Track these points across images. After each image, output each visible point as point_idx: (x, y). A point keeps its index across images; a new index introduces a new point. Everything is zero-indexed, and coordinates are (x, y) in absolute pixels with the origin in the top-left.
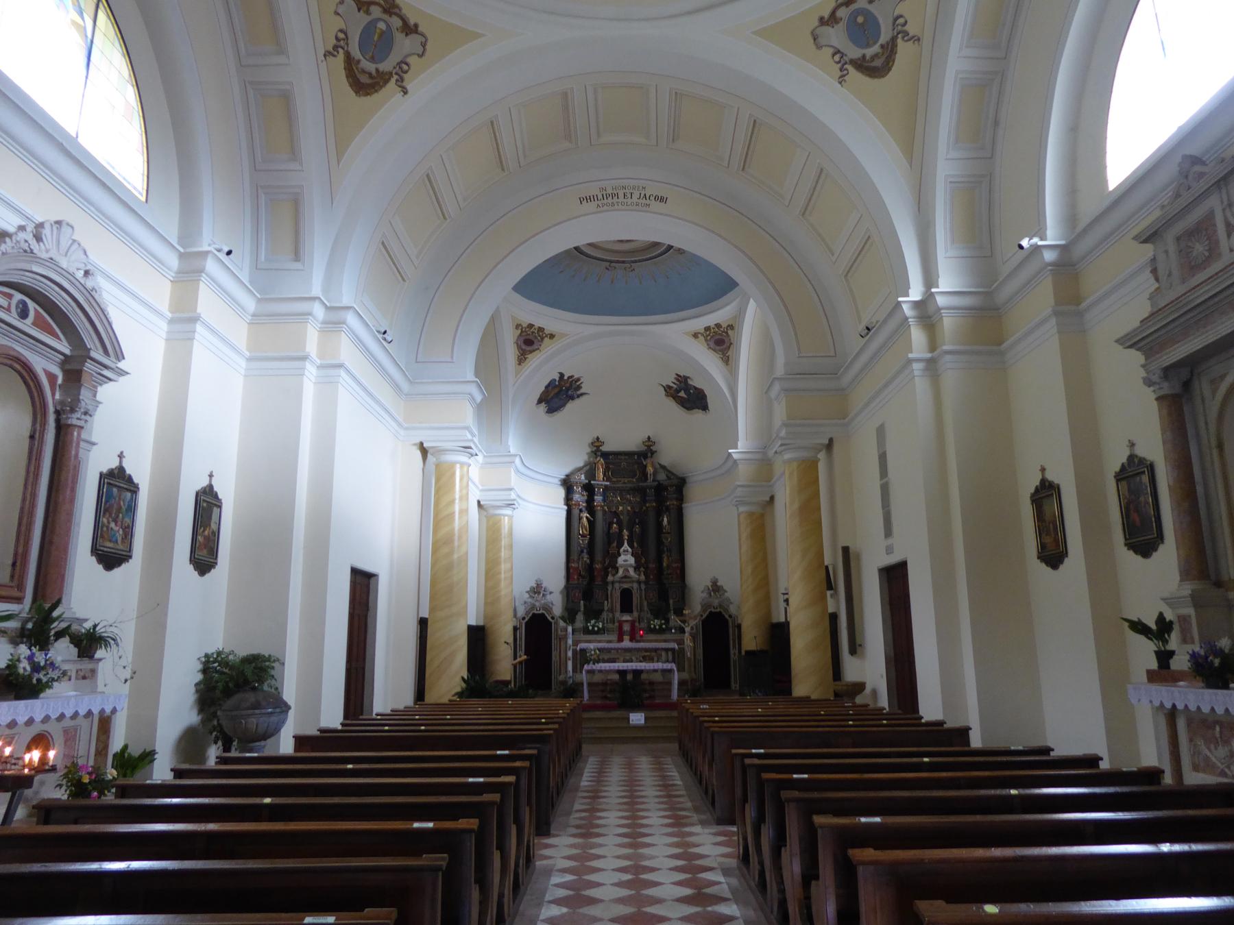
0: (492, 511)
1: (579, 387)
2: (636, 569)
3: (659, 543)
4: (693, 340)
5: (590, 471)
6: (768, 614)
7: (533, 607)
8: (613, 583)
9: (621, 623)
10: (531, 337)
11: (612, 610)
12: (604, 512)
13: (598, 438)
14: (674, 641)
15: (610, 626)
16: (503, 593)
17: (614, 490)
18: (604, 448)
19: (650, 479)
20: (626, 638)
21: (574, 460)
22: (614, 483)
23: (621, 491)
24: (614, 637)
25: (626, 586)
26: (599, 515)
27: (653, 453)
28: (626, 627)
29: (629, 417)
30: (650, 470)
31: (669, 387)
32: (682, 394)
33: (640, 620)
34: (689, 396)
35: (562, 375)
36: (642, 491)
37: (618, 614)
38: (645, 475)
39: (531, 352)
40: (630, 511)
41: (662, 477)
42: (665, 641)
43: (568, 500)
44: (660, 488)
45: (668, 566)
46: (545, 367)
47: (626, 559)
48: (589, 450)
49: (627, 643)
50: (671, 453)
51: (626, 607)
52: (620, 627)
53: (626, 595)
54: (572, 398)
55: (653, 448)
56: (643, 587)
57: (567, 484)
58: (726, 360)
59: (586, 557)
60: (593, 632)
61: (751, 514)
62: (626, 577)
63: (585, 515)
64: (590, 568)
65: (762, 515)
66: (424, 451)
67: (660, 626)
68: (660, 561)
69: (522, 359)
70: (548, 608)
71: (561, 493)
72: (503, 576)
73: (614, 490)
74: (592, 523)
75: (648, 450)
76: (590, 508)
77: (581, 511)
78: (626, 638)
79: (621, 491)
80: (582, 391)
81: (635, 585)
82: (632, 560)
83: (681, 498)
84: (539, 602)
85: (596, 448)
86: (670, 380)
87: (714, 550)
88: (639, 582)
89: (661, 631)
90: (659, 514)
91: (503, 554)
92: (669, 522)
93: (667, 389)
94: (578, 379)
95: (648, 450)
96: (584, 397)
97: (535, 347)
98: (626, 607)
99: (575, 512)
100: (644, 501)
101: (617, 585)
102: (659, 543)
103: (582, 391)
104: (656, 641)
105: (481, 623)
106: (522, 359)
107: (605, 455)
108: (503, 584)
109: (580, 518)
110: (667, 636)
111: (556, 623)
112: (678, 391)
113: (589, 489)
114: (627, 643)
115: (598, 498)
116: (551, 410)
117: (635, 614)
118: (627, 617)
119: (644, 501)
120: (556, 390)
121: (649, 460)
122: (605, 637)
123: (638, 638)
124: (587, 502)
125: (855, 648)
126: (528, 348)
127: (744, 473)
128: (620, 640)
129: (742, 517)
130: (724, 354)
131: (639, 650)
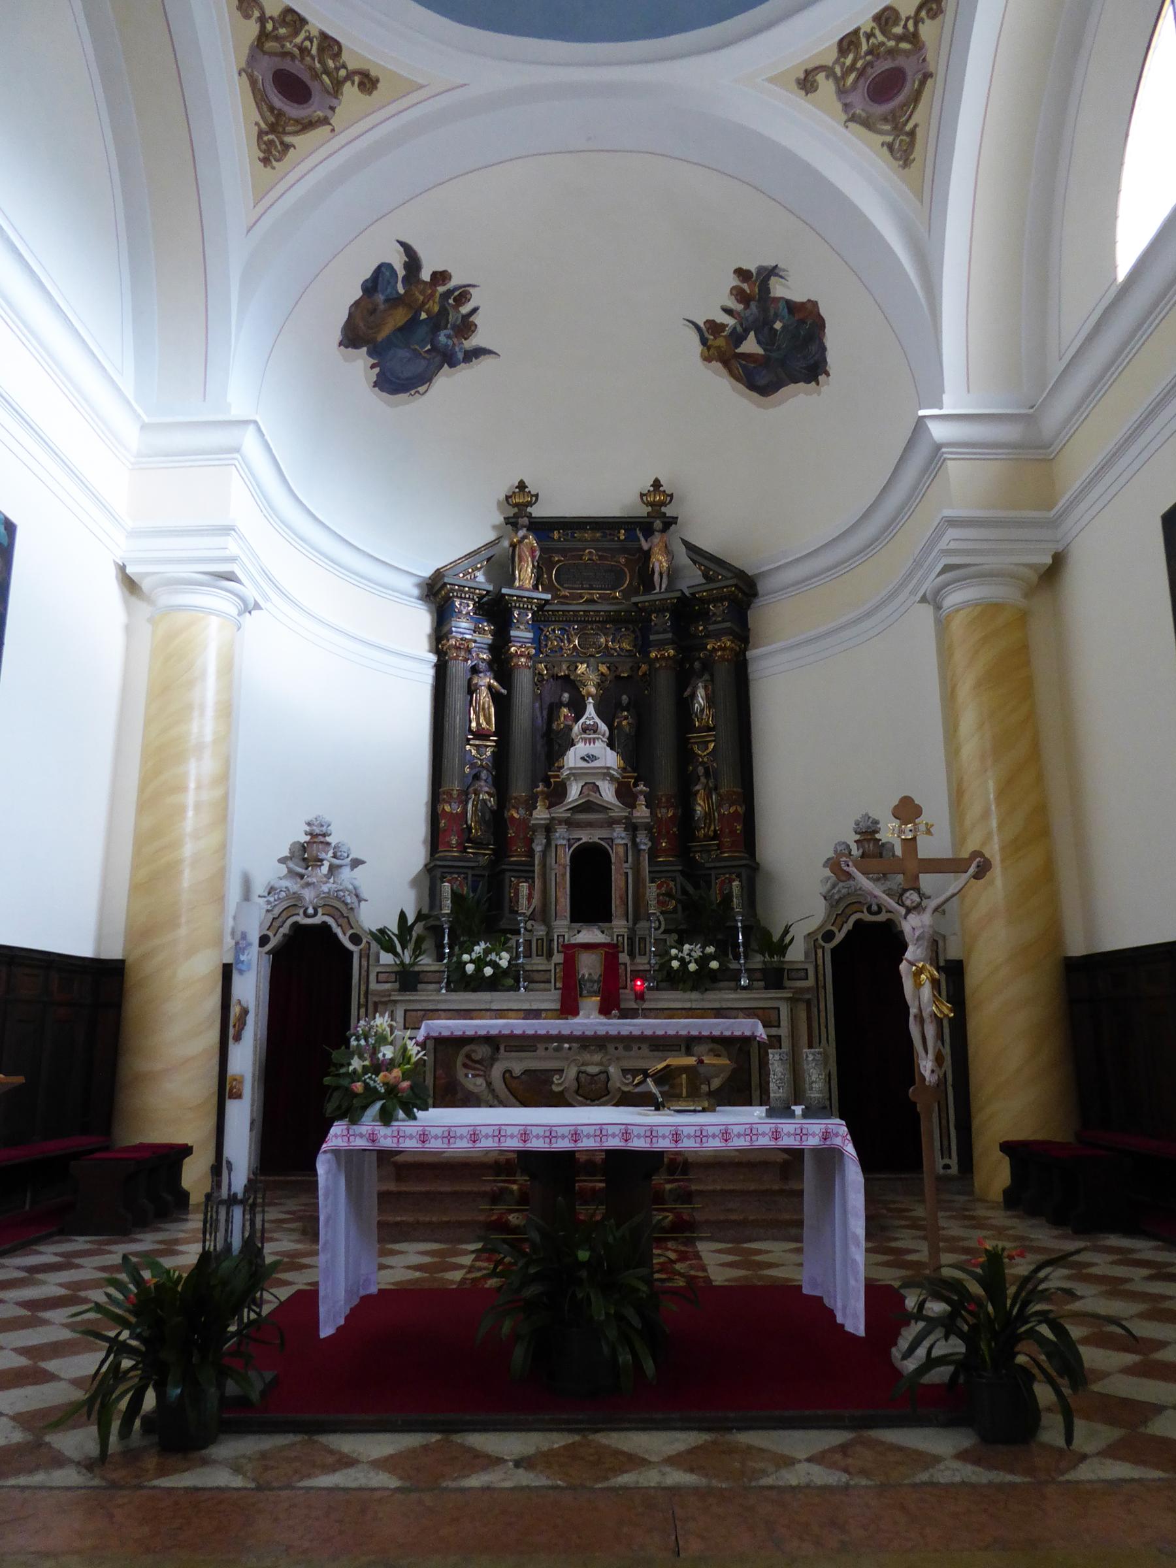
0: (166, 599)
1: (466, 327)
2: (625, 793)
3: (684, 755)
4: (798, 98)
5: (501, 565)
6: (1054, 932)
7: (295, 903)
8: (548, 829)
9: (571, 952)
10: (296, 68)
11: (543, 915)
12: (539, 680)
13: (522, 486)
14: (750, 1013)
15: (538, 963)
16: (188, 850)
17: (567, 619)
18: (538, 511)
19: (661, 584)
20: (589, 1005)
21: (458, 534)
22: (564, 600)
23: (584, 621)
24: (549, 999)
25: (586, 836)
26: (524, 680)
27: (669, 523)
28: (589, 966)
29: (607, 417)
30: (659, 561)
31: (714, 327)
32: (750, 345)
33: (635, 945)
34: (771, 343)
35: (413, 262)
36: (635, 622)
37: (561, 925)
38: (646, 579)
39: (307, 125)
40: (607, 658)
41: (692, 578)
42: (719, 1013)
43: (439, 637)
44: (686, 611)
45: (708, 816)
46: (355, 201)
47: (591, 754)
48: (499, 519)
49: (589, 1020)
50: (716, 520)
51: (591, 903)
52: (570, 965)
53: (591, 865)
54: (449, 359)
55: (669, 511)
56: (644, 842)
57: (438, 593)
58: (904, 147)
59: (485, 793)
60: (476, 983)
61: (990, 609)
62: (587, 807)
63: (485, 680)
64: (496, 821)
65: (1023, 618)
66: (130, 585)
67: (703, 961)
68: (685, 799)
69: (273, 143)
70: (342, 906)
71: (422, 620)
72: (191, 798)
73: (567, 619)
74: (503, 703)
75: (659, 513)
76: (501, 663)
77: (475, 670)
78: (589, 1005)
79: (584, 621)
80: (474, 341)
81: (619, 834)
82: (610, 759)
83: (743, 636)
84: (320, 882)
85: (519, 508)
86: (714, 301)
87: (846, 744)
88: (632, 828)
89: (703, 980)
90: (683, 680)
91: (204, 727)
92: (710, 699)
93: (709, 332)
94: (462, 295)
95: (659, 513)
96: (485, 363)
97: (313, 110)
98: (591, 903)
99: (459, 669)
100: (643, 646)
101: (561, 834)
102: (684, 755)
103: (474, 341)
104: (690, 1013)
105: (114, 952)
106: (273, 143)
107: (543, 528)
108: (190, 821)
109: (471, 690)
110: (724, 997)
111: (365, 954)
112: (738, 338)
113: (495, 611)
114: (589, 1020)
115: (521, 634)
116: (395, 382)
117: (620, 925)
118: (590, 935)
119: (643, 646)
120: (400, 317)
121: (657, 538)
122: (521, 999)
123: (628, 1000)
124: (492, 648)
125: (238, 1038)
126: (293, 111)
127: (964, 486)
128: (569, 1008)
129: (957, 625)
130: (898, 129)
131: (628, 1041)
